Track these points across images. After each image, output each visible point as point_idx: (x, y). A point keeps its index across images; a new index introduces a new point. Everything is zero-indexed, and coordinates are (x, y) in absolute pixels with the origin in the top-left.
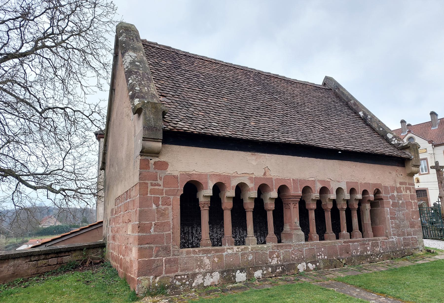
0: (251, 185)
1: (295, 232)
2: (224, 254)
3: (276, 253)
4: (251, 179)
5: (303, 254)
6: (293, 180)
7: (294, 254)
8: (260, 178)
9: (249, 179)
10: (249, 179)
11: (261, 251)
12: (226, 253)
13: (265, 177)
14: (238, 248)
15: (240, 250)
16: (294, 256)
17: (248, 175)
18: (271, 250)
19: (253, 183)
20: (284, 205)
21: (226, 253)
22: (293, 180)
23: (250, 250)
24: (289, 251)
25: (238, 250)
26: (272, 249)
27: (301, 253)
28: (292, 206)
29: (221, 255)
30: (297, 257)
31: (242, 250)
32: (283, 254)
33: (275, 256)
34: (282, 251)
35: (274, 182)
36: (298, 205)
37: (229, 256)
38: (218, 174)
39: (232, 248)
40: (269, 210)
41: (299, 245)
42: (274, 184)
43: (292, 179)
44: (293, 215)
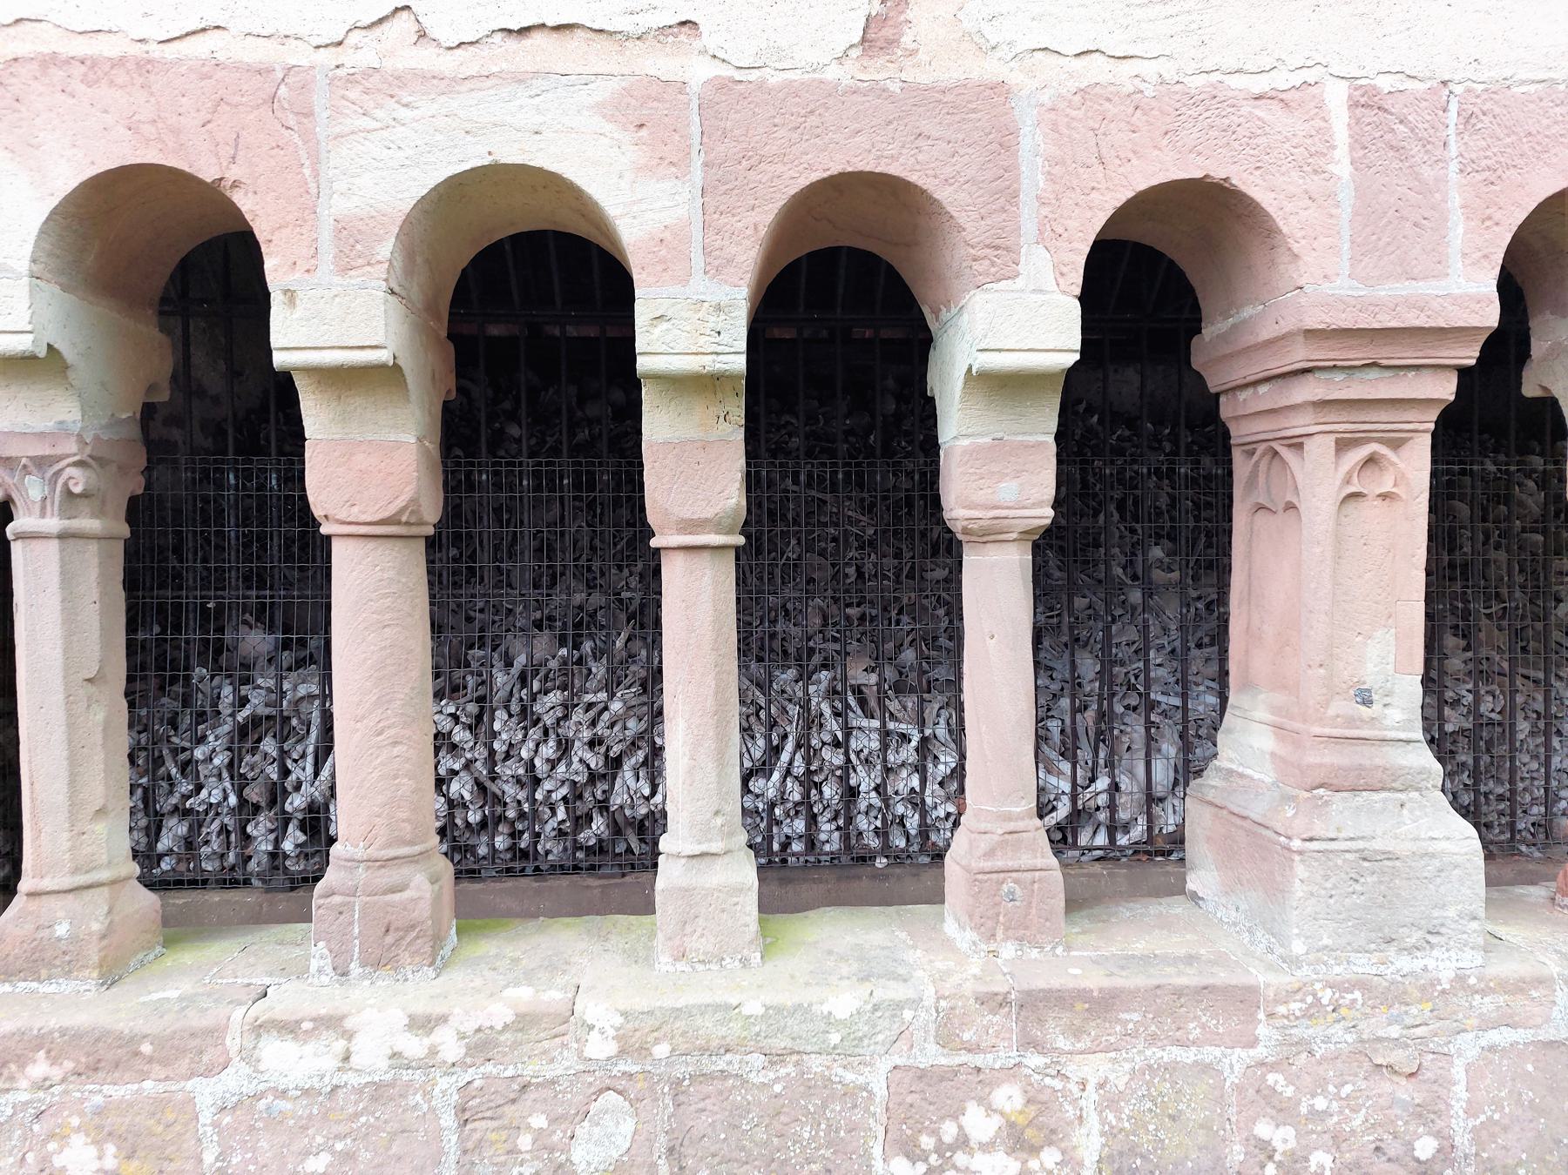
0: (277, 67)
1: (1346, 817)
2: (206, 1093)
3: (1009, 1097)
4: (645, 111)
5: (1427, 1113)
6: (1366, 102)
7: (1283, 1112)
8: (810, 102)
9: (613, 110)
10: (613, 110)
11: (775, 1058)
12: (233, 1081)
13: (879, 71)
14: (422, 1024)
15: (452, 1050)
16: (1283, 1138)
17: (599, 56)
18: (931, 1055)
19: (677, 165)
20: (1241, 467)
21: (233, 1081)
22: (1366, 102)
23: (600, 1047)
24: (1205, 1068)
25: (414, 1046)
26: (946, 1040)
27: (1405, 1091)
28: (1319, 474)
29: (159, 1105)
30: (1338, 1140)
31: (482, 1046)
32: (1111, 1102)
33: (979, 1124)
34: (1094, 1068)
35: (1032, 144)
36: (1414, 467)
37: (274, 1121)
38: (107, 48)
39: (331, 1023)
40: (990, 535)
41: (1390, 996)
42: (1033, 178)
43: (1336, 96)
44: (1337, 568)
